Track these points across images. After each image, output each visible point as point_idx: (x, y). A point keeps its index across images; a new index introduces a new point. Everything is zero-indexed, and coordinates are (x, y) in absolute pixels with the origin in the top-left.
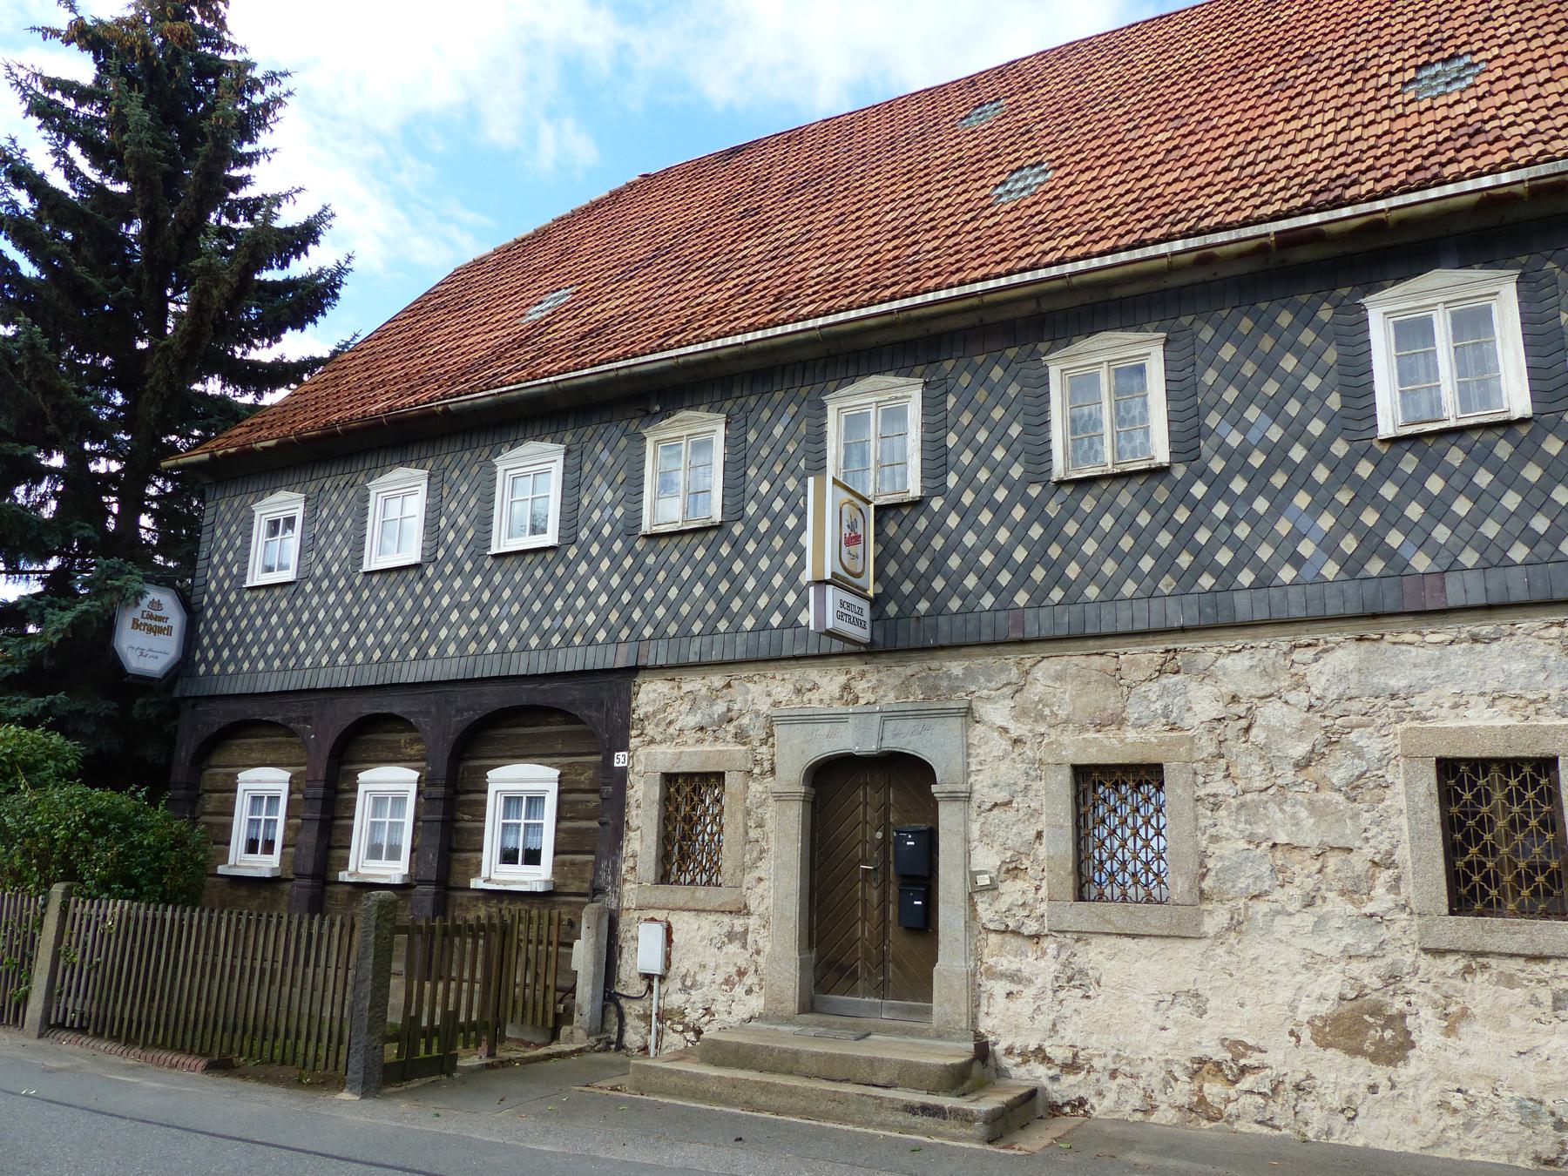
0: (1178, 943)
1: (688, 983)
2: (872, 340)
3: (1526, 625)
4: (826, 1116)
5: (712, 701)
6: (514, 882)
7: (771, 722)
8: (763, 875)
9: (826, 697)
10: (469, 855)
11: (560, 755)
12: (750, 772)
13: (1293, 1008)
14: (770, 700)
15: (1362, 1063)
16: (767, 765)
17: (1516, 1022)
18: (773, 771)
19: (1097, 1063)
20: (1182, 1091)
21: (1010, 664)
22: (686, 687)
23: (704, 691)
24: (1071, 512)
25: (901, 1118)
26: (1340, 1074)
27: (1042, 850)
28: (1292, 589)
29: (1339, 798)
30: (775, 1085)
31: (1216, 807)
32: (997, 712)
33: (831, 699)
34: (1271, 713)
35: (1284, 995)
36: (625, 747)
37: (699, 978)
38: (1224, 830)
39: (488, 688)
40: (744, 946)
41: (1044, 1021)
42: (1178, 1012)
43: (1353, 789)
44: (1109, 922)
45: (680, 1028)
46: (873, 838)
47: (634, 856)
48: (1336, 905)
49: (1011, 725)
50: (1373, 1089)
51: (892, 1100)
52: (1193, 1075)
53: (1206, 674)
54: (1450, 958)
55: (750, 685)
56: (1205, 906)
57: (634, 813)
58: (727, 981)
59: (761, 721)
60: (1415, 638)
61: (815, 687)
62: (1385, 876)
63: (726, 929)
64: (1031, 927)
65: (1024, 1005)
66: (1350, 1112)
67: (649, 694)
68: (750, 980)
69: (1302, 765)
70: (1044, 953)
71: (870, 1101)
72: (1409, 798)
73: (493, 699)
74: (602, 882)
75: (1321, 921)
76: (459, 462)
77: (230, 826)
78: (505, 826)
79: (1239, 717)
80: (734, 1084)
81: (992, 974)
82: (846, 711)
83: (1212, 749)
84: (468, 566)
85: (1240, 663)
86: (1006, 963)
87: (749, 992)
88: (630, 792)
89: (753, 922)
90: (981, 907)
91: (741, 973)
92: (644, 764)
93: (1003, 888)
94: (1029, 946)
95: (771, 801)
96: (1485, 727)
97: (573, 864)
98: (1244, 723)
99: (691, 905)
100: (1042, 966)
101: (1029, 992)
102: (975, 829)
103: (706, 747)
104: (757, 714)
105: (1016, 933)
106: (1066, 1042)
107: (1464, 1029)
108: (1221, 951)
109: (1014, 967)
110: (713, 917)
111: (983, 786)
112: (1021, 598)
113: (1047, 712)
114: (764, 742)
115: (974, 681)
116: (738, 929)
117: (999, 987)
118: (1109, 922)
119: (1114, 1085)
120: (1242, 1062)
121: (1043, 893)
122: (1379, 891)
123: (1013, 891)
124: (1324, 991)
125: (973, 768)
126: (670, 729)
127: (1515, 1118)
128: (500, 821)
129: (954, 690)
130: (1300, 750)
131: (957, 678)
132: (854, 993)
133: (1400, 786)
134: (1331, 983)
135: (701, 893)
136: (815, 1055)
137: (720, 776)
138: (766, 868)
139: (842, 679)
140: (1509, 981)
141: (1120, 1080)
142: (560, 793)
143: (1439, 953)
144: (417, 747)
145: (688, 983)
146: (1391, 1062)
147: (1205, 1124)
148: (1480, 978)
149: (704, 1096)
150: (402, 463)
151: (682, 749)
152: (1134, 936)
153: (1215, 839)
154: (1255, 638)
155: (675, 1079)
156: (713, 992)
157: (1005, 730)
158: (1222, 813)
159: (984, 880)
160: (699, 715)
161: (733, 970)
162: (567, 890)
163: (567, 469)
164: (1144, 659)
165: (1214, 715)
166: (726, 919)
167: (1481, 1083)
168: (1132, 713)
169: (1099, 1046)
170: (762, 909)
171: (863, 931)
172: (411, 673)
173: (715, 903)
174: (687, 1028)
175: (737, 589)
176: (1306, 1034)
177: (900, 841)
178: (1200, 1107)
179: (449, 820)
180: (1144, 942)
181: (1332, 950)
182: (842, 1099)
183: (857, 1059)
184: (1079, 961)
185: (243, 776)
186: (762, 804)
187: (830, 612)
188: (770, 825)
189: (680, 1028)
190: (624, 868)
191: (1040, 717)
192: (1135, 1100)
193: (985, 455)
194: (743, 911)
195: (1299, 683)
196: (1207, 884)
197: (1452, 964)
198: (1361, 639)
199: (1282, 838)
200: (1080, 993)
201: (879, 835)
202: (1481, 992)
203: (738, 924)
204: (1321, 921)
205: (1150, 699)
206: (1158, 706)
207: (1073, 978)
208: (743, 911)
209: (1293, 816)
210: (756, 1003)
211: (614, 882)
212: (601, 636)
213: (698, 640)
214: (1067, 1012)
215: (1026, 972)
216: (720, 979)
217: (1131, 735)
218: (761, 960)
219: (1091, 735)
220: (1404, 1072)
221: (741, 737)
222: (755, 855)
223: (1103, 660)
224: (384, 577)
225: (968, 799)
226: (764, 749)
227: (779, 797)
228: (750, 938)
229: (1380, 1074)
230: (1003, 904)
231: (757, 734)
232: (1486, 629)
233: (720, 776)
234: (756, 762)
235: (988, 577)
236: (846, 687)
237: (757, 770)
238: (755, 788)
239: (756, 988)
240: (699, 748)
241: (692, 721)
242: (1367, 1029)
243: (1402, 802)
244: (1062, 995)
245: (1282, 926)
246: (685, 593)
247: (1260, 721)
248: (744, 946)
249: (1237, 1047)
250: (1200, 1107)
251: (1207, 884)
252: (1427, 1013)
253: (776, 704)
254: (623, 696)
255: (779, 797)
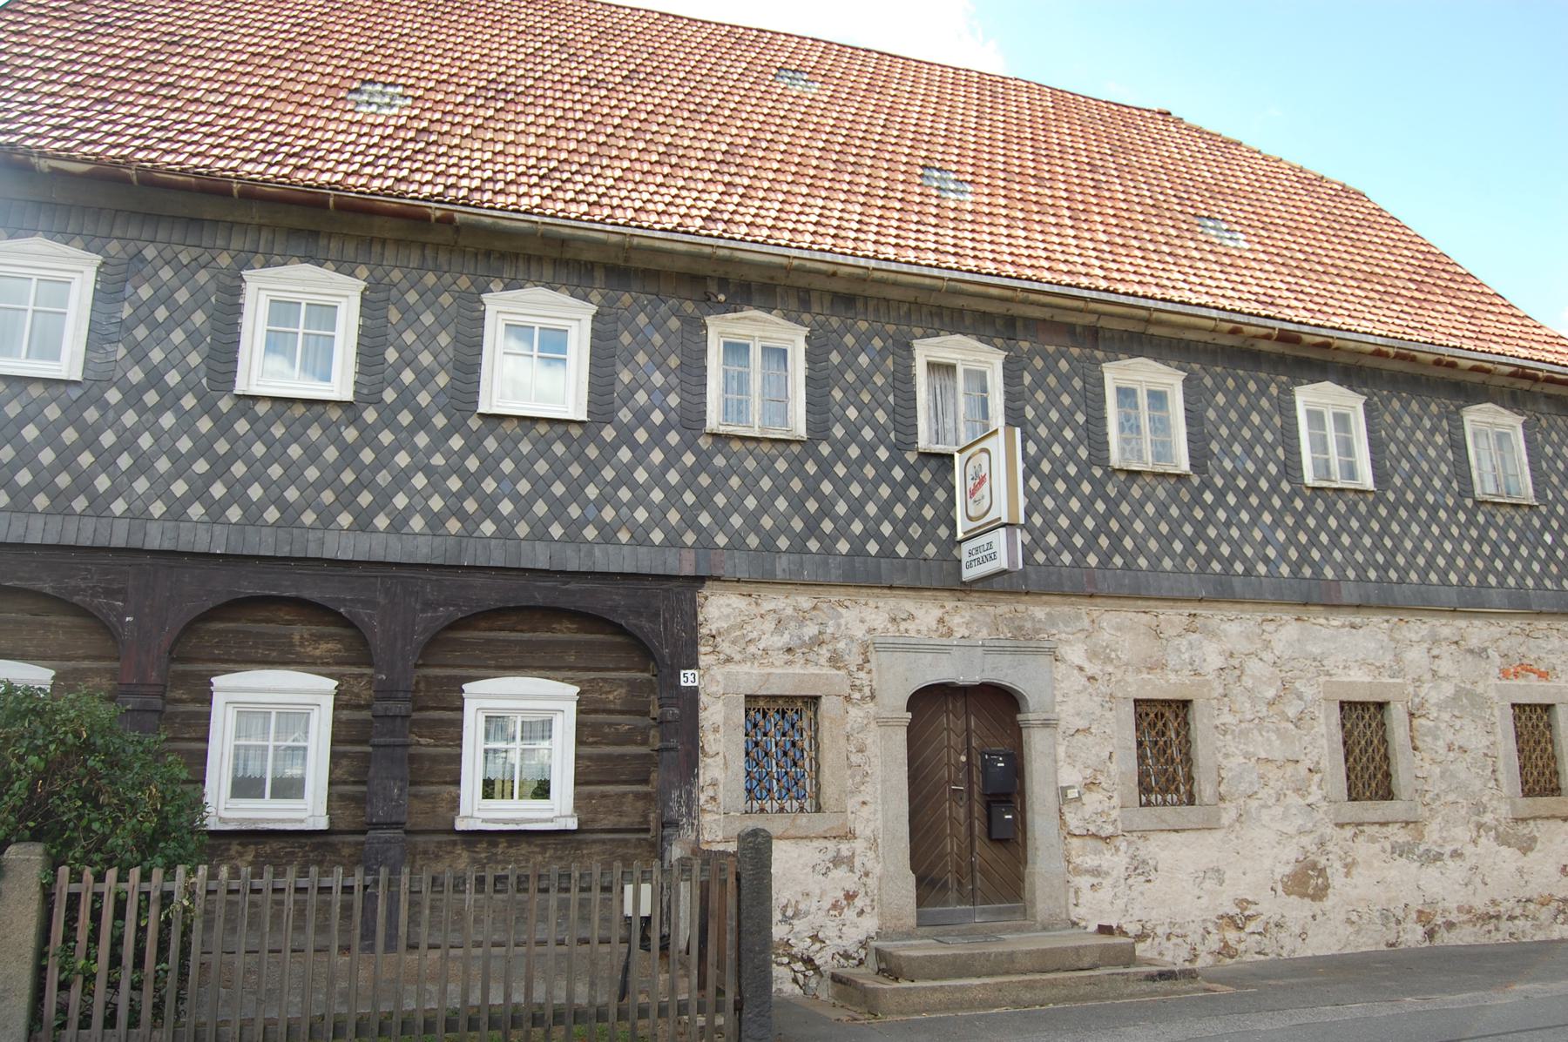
0: (1206, 833)
1: (790, 913)
2: (960, 302)
3: (1375, 619)
4: (1085, 998)
5: (802, 622)
6: (537, 821)
7: (865, 648)
8: (868, 799)
9: (924, 629)
10: (434, 788)
11: (571, 668)
12: (848, 698)
13: (1273, 872)
14: (864, 627)
15: (1307, 901)
16: (867, 691)
17: (1376, 864)
18: (873, 697)
19: (1159, 931)
20: (1214, 942)
21: (1085, 611)
22: (767, 605)
23: (789, 611)
24: (1123, 495)
25: (1144, 986)
26: (1297, 910)
27: (1113, 767)
28: (493, 542)
29: (1292, 726)
30: (1035, 981)
31: (1225, 733)
32: (1075, 653)
33: (929, 630)
34: (1254, 666)
35: (1267, 863)
36: (694, 665)
37: (802, 906)
38: (1232, 749)
39: (478, 580)
40: (852, 870)
41: (1120, 903)
42: (1208, 885)
43: (1298, 722)
44: (1164, 821)
45: (786, 960)
46: (957, 761)
47: (714, 784)
48: (1293, 799)
49: (1086, 665)
50: (1314, 917)
51: (1135, 974)
52: (1218, 927)
53: (1213, 634)
54: (1348, 828)
55: (843, 611)
56: (1222, 805)
57: (711, 737)
58: (834, 906)
59: (856, 649)
60: (1322, 621)
61: (911, 617)
62: (1317, 777)
63: (831, 854)
64: (1108, 830)
65: (1105, 894)
66: (1303, 935)
67: (719, 609)
68: (859, 902)
69: (1271, 704)
70: (1117, 849)
71: (1119, 978)
72: (1327, 726)
73: (489, 594)
74: (674, 814)
75: (1287, 808)
76: (424, 287)
77: (205, 753)
78: (486, 751)
79: (1233, 668)
80: (999, 988)
81: (1078, 871)
82: (946, 640)
83: (1221, 690)
84: (440, 421)
85: (1233, 628)
86: (1090, 861)
87: (862, 912)
88: (702, 715)
89: (859, 845)
90: (1068, 817)
91: (850, 897)
92: (720, 685)
93: (1085, 798)
94: (1101, 845)
95: (873, 725)
96: (1360, 682)
97: (604, 796)
98: (1237, 672)
99: (792, 832)
100: (1115, 861)
101: (1107, 882)
102: (1061, 751)
103: (797, 669)
104: (852, 639)
105: (1095, 836)
106: (1135, 918)
107: (1354, 872)
108: (1232, 836)
109: (1096, 863)
110: (816, 843)
111: (1067, 715)
112: (522, 529)
113: (1113, 655)
114: (860, 668)
115: (1054, 625)
116: (845, 852)
117: (1084, 882)
118: (1164, 821)
119: (1169, 944)
120: (1247, 913)
121: (1116, 801)
122: (1314, 788)
123: (1093, 800)
124: (1283, 860)
125: (1059, 699)
126: (744, 646)
127: (1378, 921)
128: (481, 745)
129: (1037, 631)
130: (1270, 693)
131: (1040, 621)
132: (945, 903)
133: (1322, 720)
134: (1291, 853)
135: (803, 819)
136: (1028, 953)
137: (814, 701)
138: (869, 792)
139: (938, 613)
140: (1373, 839)
141: (1174, 940)
142: (579, 712)
143: (1341, 826)
144: (324, 646)
145: (790, 913)
146: (1321, 899)
147: (1228, 961)
148: (1361, 838)
149: (971, 1005)
150: (308, 258)
151: (769, 670)
152: (1176, 831)
153: (1226, 756)
154: (1242, 611)
155: (939, 996)
156: (818, 918)
157: (1081, 669)
158: (1229, 737)
159: (1072, 794)
160: (786, 637)
161: (841, 895)
162: (597, 826)
163: (596, 334)
164: (1176, 619)
165: (1220, 665)
166: (831, 844)
167: (1363, 904)
168: (1173, 661)
169: (1158, 917)
170: (868, 832)
171: (950, 845)
172: (342, 544)
173: (820, 830)
174: (793, 958)
175: (826, 510)
176: (1280, 889)
177: (992, 763)
178: (1226, 950)
179: (396, 746)
180: (1184, 835)
181: (1291, 830)
182: (1092, 982)
183: (1065, 950)
184: (1142, 854)
185: (217, 681)
186: (864, 728)
187: (999, 552)
188: (873, 750)
189: (786, 960)
190: (703, 798)
191: (1109, 660)
192: (1184, 953)
193: (648, 384)
194: (850, 835)
195: (1267, 645)
196: (1222, 789)
197: (1349, 832)
198: (1298, 619)
199: (1263, 755)
200: (1142, 878)
201: (963, 758)
202: (1363, 849)
203: (845, 848)
204: (1287, 808)
205: (1181, 650)
206: (1186, 656)
207: (1140, 868)
208: (850, 835)
209: (1268, 739)
210: (870, 924)
211: (689, 814)
212: (657, 536)
213: (784, 558)
214: (1134, 894)
215: (1105, 868)
216: (827, 904)
217: (1172, 677)
218: (869, 881)
219: (1145, 676)
220: (1328, 903)
221: (835, 660)
222: (858, 779)
223: (1147, 617)
224: (279, 407)
225: (1055, 726)
226: (862, 674)
227: (883, 722)
228: (857, 862)
229: (1317, 906)
230: (1088, 810)
231: (854, 660)
232: (1358, 620)
233: (814, 701)
234: (853, 687)
235: (275, 490)
236: (941, 621)
237: (856, 695)
238: (854, 712)
239: (867, 909)
240: (790, 670)
241: (784, 640)
242: (1307, 881)
243: (1323, 730)
244: (1130, 881)
245: (1265, 816)
246: (765, 506)
247: (1248, 672)
248: (852, 870)
249: (1242, 903)
250: (1226, 950)
251: (1222, 789)
252: (1338, 865)
253: (871, 630)
254: (686, 607)
255: (883, 722)
